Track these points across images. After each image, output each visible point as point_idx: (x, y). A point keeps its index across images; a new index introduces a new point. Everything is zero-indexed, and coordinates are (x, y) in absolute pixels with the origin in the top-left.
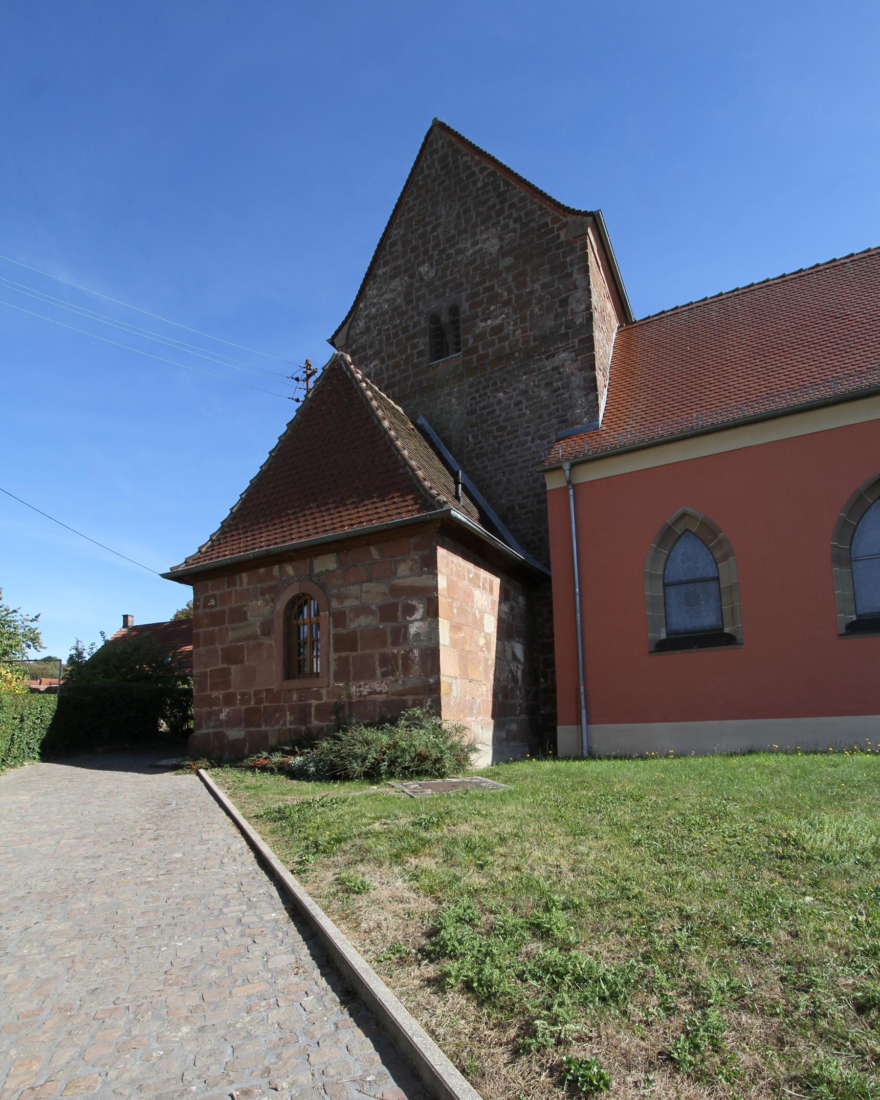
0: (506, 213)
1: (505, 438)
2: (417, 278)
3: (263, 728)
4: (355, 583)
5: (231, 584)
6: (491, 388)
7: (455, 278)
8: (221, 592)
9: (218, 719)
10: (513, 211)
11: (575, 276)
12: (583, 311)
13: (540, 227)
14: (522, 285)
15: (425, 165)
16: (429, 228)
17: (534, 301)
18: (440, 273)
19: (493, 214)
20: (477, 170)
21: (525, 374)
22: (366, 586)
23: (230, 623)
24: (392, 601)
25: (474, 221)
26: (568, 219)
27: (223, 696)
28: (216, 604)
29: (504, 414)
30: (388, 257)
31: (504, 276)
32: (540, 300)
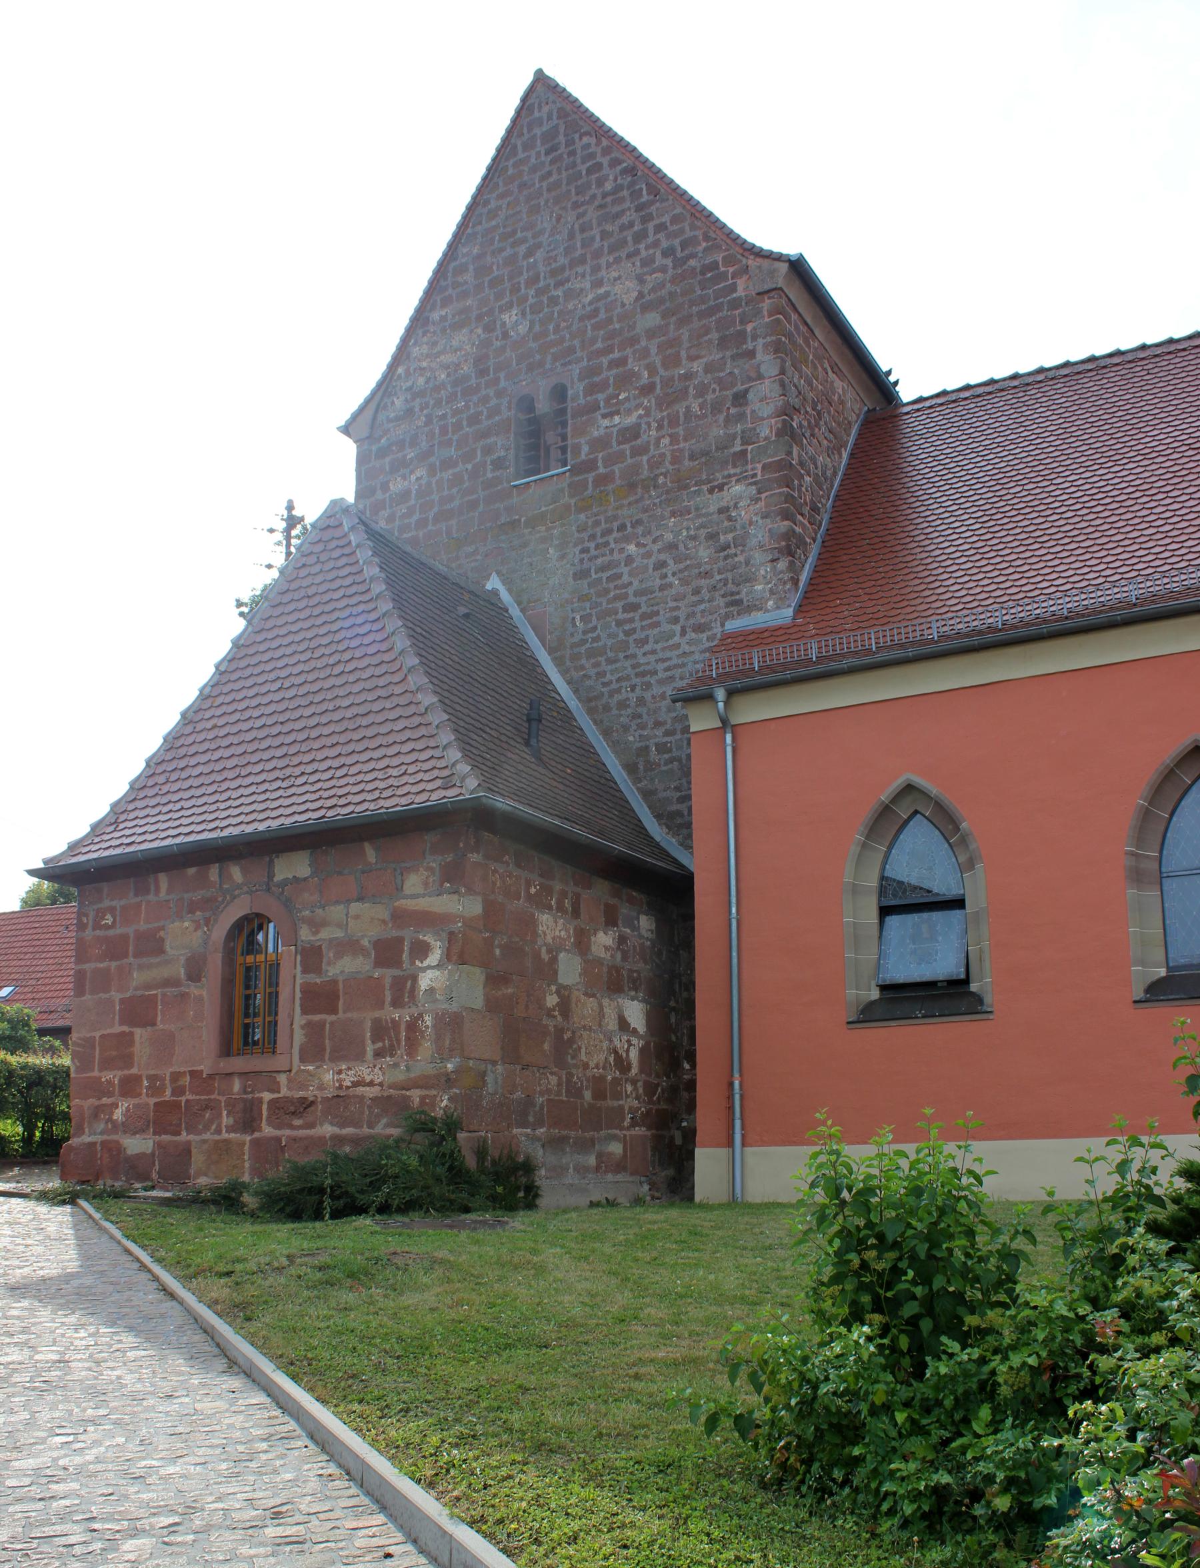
0: (651, 239)
1: (637, 624)
2: (499, 332)
3: (184, 1136)
4: (337, 902)
5: (142, 890)
6: (615, 535)
7: (562, 340)
8: (123, 902)
9: (110, 1120)
10: (661, 236)
11: (759, 356)
12: (769, 417)
13: (706, 269)
14: (672, 361)
15: (519, 143)
16: (522, 249)
17: (692, 391)
18: (537, 328)
19: (629, 238)
20: (605, 161)
21: (673, 514)
22: (355, 907)
23: (135, 956)
24: (395, 933)
25: (597, 245)
26: (750, 262)
27: (120, 1080)
28: (114, 922)
29: (636, 583)
30: (450, 291)
31: (643, 343)
32: (702, 391)
